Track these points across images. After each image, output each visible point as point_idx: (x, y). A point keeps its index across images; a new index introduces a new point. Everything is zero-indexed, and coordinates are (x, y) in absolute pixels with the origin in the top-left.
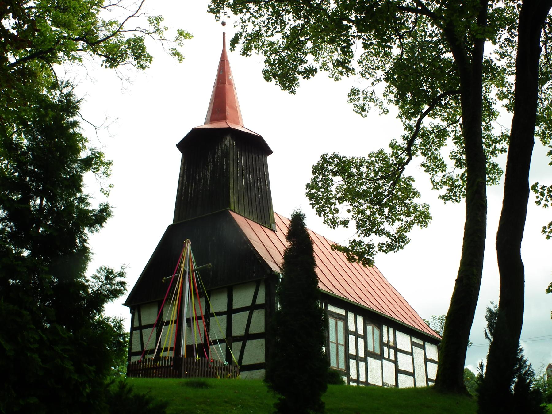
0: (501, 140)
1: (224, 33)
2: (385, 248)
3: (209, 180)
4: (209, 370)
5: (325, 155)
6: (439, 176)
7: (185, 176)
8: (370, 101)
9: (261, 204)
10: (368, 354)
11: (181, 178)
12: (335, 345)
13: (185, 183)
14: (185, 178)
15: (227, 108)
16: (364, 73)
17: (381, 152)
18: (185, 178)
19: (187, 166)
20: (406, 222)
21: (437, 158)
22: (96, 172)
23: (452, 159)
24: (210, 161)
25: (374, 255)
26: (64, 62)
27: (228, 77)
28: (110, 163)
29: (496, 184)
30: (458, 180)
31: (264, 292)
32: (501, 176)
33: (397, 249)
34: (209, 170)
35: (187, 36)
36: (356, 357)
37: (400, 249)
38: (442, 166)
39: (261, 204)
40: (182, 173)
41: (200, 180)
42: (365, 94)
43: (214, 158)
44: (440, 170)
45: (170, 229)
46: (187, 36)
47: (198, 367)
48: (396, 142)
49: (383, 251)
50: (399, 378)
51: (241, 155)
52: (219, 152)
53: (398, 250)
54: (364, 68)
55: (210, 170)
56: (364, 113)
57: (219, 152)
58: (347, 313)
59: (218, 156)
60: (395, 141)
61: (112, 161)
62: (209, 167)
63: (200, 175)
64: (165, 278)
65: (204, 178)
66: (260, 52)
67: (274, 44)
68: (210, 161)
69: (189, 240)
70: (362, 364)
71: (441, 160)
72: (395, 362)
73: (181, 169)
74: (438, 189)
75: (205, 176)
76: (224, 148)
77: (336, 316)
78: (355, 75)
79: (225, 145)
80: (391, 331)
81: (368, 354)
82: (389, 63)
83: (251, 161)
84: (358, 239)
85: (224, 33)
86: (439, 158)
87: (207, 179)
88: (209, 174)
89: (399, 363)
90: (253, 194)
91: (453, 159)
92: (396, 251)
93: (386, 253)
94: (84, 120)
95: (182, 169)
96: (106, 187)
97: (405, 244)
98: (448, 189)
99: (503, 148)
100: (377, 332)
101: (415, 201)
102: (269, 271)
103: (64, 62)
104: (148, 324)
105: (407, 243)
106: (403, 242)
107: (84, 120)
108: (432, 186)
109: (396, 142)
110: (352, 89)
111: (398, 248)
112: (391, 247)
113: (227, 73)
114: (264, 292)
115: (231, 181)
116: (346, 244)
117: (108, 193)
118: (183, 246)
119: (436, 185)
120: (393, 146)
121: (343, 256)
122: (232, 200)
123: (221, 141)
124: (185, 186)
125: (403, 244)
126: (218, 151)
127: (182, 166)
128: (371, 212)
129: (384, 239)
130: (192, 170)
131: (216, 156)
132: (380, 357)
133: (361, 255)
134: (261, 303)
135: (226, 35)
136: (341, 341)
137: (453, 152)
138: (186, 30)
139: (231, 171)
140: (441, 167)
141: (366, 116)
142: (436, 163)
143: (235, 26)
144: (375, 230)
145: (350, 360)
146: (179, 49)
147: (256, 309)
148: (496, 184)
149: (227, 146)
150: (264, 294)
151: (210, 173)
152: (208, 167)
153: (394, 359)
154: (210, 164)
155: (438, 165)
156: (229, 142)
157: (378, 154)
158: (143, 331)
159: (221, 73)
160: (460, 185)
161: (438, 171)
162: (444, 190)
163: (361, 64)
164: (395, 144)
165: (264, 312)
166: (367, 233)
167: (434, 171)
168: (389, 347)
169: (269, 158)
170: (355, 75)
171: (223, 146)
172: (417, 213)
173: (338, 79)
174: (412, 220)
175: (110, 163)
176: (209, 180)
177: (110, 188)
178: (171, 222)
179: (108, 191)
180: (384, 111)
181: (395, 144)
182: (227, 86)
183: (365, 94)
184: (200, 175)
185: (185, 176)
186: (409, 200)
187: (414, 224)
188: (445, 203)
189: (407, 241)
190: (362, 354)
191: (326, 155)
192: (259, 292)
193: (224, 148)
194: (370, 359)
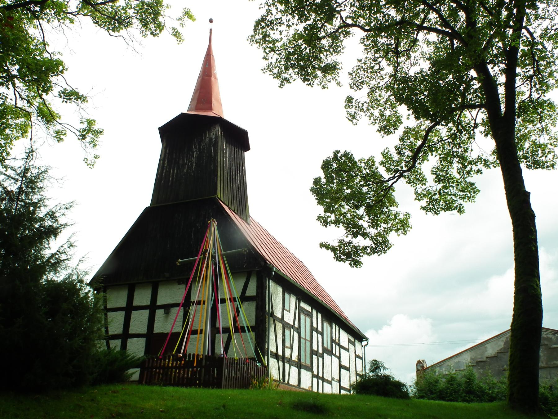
0: (477, 162)
1: (211, 30)
2: (369, 251)
3: (194, 166)
4: (243, 365)
5: (336, 151)
6: (420, 188)
7: (166, 160)
8: (360, 111)
9: (240, 197)
10: (325, 350)
11: (162, 162)
12: (304, 341)
13: (166, 167)
14: (166, 162)
15: (213, 99)
16: (352, 85)
17: (371, 159)
18: (166, 162)
19: (169, 150)
20: (385, 228)
21: (417, 172)
22: (83, 140)
23: (432, 174)
24: (195, 148)
25: (361, 256)
26: (53, 21)
27: (214, 71)
28: (101, 132)
29: (472, 202)
30: (436, 194)
31: (256, 284)
32: (476, 194)
33: (380, 253)
34: (195, 157)
35: (190, 17)
36: (316, 353)
37: (383, 253)
38: (423, 180)
39: (240, 197)
40: (163, 156)
41: (183, 165)
42: (357, 103)
43: (200, 145)
44: (420, 183)
45: (147, 212)
46: (190, 17)
47: (245, 365)
48: (389, 151)
49: (367, 254)
50: (341, 373)
51: (227, 146)
52: (207, 140)
53: (381, 254)
54: (353, 80)
55: (196, 156)
56: (354, 121)
57: (207, 140)
58: (312, 310)
59: (206, 144)
60: (387, 149)
61: (103, 130)
62: (195, 154)
63: (183, 161)
64: (180, 260)
65: (188, 164)
66: (261, 47)
67: (277, 41)
68: (195, 148)
69: (215, 220)
70: (321, 359)
71: (421, 174)
72: (339, 358)
73: (161, 152)
74: (419, 200)
75: (189, 161)
76: (212, 136)
77: (305, 313)
78: (340, 86)
79: (214, 134)
80: (337, 328)
81: (325, 350)
82: (374, 80)
83: (233, 154)
84: (347, 240)
85: (211, 30)
86: (419, 172)
87: (192, 165)
88: (194, 160)
89: (342, 359)
90: (235, 186)
91: (434, 174)
92: (380, 255)
93: (370, 256)
94: (68, 85)
95: (163, 152)
96: (90, 158)
97: (388, 249)
98: (427, 202)
99: (479, 170)
100: (329, 328)
101: (394, 209)
102: (263, 263)
103: (53, 21)
104: (115, 307)
105: (390, 247)
106: (386, 246)
107: (68, 85)
108: (415, 197)
109: (389, 151)
110: (348, 96)
111: (381, 251)
112: (374, 251)
113: (213, 67)
114: (256, 284)
115: (219, 169)
116: (335, 244)
117: (92, 163)
118: (206, 227)
119: (419, 196)
120: (385, 154)
121: (331, 254)
122: (219, 188)
123: (210, 130)
124: (166, 170)
125: (386, 249)
126: (205, 139)
127: (164, 150)
128: (351, 215)
129: (368, 242)
130: (174, 155)
131: (203, 144)
132: (330, 353)
133: (348, 255)
134: (252, 295)
135: (213, 31)
136: (308, 338)
137: (434, 167)
138: (193, 12)
139: (219, 160)
140: (421, 181)
141: (356, 124)
142: (416, 176)
143: (260, 8)
144: (361, 233)
145: (314, 356)
146: (180, 29)
147: (246, 301)
148: (472, 202)
149: (216, 135)
150: (255, 287)
151: (196, 159)
152: (193, 154)
153: (338, 355)
154: (196, 151)
155: (419, 179)
156: (218, 131)
157: (369, 160)
158: (109, 314)
159: (207, 66)
160: (437, 199)
161: (419, 184)
162: (424, 203)
163: (351, 76)
164: (387, 153)
165: (255, 305)
166: (355, 235)
167: (415, 183)
168: (336, 344)
169: (247, 154)
170: (340, 86)
171: (211, 134)
172: (397, 220)
173: (324, 88)
174: (389, 227)
175: (101, 132)
176: (194, 166)
177: (95, 159)
178: (148, 204)
179: (93, 161)
180: (372, 122)
181: (387, 153)
182: (213, 79)
183: (357, 103)
184: (183, 161)
185: (166, 160)
186: (387, 208)
187: (391, 231)
188: (427, 214)
189: (390, 246)
190: (320, 351)
191: (339, 152)
192: (250, 283)
193: (212, 136)
194: (325, 355)
